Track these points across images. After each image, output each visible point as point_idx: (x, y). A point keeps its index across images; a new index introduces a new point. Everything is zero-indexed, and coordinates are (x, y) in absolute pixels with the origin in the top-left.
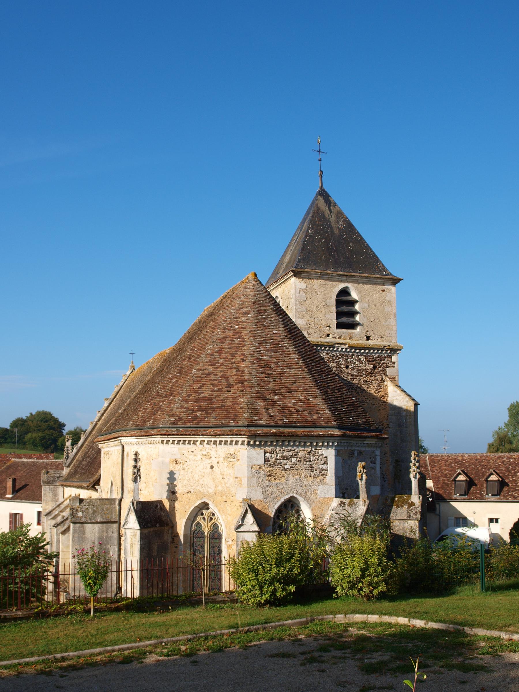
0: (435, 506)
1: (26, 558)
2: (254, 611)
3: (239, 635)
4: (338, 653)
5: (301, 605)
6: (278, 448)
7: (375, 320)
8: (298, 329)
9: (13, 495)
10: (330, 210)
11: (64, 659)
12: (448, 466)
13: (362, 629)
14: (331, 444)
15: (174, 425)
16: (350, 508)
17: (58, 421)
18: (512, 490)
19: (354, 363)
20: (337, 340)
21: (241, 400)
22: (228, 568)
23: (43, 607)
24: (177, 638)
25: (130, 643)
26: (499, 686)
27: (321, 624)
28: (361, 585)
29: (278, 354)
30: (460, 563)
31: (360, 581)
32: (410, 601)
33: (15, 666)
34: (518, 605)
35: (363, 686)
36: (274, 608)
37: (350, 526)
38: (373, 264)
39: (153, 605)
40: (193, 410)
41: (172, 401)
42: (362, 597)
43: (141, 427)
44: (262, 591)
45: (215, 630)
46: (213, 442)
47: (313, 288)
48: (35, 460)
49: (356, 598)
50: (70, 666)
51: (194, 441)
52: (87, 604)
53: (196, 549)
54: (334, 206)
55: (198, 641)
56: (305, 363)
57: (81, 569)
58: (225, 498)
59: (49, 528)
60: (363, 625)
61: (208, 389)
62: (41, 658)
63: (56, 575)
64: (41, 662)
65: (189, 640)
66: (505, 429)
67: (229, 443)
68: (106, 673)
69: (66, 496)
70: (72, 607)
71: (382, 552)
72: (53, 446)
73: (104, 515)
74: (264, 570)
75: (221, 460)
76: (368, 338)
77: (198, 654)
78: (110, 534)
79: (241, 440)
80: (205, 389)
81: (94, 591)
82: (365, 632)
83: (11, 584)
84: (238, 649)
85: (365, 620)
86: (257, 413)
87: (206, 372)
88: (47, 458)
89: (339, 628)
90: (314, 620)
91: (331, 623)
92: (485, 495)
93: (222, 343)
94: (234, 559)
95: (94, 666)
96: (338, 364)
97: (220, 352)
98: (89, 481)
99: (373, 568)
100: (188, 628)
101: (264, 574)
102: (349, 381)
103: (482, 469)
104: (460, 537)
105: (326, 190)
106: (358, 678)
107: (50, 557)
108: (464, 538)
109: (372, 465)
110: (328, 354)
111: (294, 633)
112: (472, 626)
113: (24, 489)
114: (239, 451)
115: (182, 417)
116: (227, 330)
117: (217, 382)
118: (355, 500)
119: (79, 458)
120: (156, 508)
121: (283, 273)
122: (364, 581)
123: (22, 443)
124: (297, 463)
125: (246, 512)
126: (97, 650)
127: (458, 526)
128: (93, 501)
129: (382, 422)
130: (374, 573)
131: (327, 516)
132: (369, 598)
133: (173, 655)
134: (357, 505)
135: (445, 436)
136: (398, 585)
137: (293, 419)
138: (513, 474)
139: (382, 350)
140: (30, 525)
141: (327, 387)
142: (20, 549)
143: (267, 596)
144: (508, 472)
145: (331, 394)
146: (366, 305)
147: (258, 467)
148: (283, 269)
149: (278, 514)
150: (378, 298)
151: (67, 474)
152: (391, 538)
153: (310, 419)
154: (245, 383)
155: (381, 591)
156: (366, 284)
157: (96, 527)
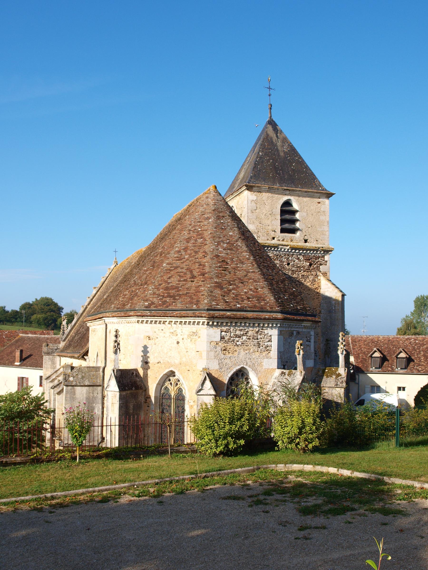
0: (355, 377)
1: (29, 413)
2: (211, 460)
3: (198, 480)
4: (279, 497)
5: (249, 455)
6: (232, 328)
7: (311, 226)
8: (250, 232)
9: (20, 363)
10: (277, 137)
11: (53, 498)
12: (366, 345)
13: (299, 476)
14: (275, 325)
15: (148, 308)
16: (289, 377)
17: (57, 305)
18: (417, 365)
19: (294, 261)
20: (281, 243)
21: (202, 289)
22: (190, 425)
23: (38, 454)
24: (147, 482)
25: (108, 485)
26: (414, 528)
27: (265, 471)
28: (299, 440)
29: (233, 252)
30: (378, 423)
31: (298, 437)
32: (338, 454)
33: (12, 503)
34: (427, 459)
35: (301, 525)
36: (227, 457)
37: (290, 392)
38: (311, 181)
39: (128, 454)
40: (163, 296)
41: (146, 289)
42: (299, 450)
43: (121, 310)
44: (217, 444)
45: (178, 475)
46: (179, 322)
47: (262, 200)
48: (38, 336)
49: (294, 451)
50: (58, 504)
51: (164, 321)
52: (74, 453)
53: (164, 408)
54: (280, 133)
55: (164, 484)
56: (255, 260)
57: (69, 424)
58: (188, 368)
59: (48, 389)
60: (300, 473)
61: (175, 280)
62: (34, 497)
63: (53, 427)
64: (34, 500)
65: (157, 484)
66: (411, 317)
67: (192, 323)
68: (87, 511)
69: (62, 364)
70: (61, 455)
71: (316, 414)
72: (53, 325)
73: (91, 380)
74: (219, 427)
75: (185, 337)
76: (306, 241)
77: (164, 495)
78: (95, 395)
79: (202, 321)
80: (173, 280)
81: (79, 442)
82: (301, 480)
83: (17, 433)
84: (197, 492)
85: (302, 469)
86: (215, 300)
87: (174, 266)
88: (48, 334)
89: (280, 475)
90: (260, 468)
91: (273, 471)
92: (395, 369)
93: (188, 242)
94: (194, 418)
95: (78, 504)
96: (281, 261)
97: (186, 249)
98: (80, 353)
99: (309, 426)
100: (156, 474)
101: (219, 430)
102: (290, 276)
103: (393, 348)
104: (378, 402)
105: (274, 120)
106: (296, 519)
107: (48, 412)
108: (382, 403)
109: (307, 343)
110: (273, 253)
111: (243, 479)
112: (390, 476)
113: (29, 358)
114: (200, 330)
115: (154, 302)
116: (192, 232)
117: (183, 274)
118: (294, 371)
119: (72, 334)
120: (132, 375)
121: (238, 187)
122: (301, 437)
123: (28, 322)
124: (247, 340)
125: (205, 379)
126: (81, 491)
127: (373, 392)
128: (82, 368)
129: (315, 309)
130: (309, 431)
131: (271, 384)
132: (304, 451)
133: (143, 496)
134: (295, 375)
135: (364, 322)
136: (328, 440)
137: (244, 304)
138: (418, 352)
139: (317, 251)
140: (32, 387)
141: (273, 280)
142: (25, 405)
143: (221, 448)
144: (414, 350)
145: (275, 285)
146: (305, 214)
147: (215, 343)
148: (238, 184)
149: (231, 381)
150: (314, 209)
151: (63, 346)
152: (324, 403)
153: (258, 305)
154: (206, 275)
155: (314, 445)
156: (305, 197)
157: (85, 390)
